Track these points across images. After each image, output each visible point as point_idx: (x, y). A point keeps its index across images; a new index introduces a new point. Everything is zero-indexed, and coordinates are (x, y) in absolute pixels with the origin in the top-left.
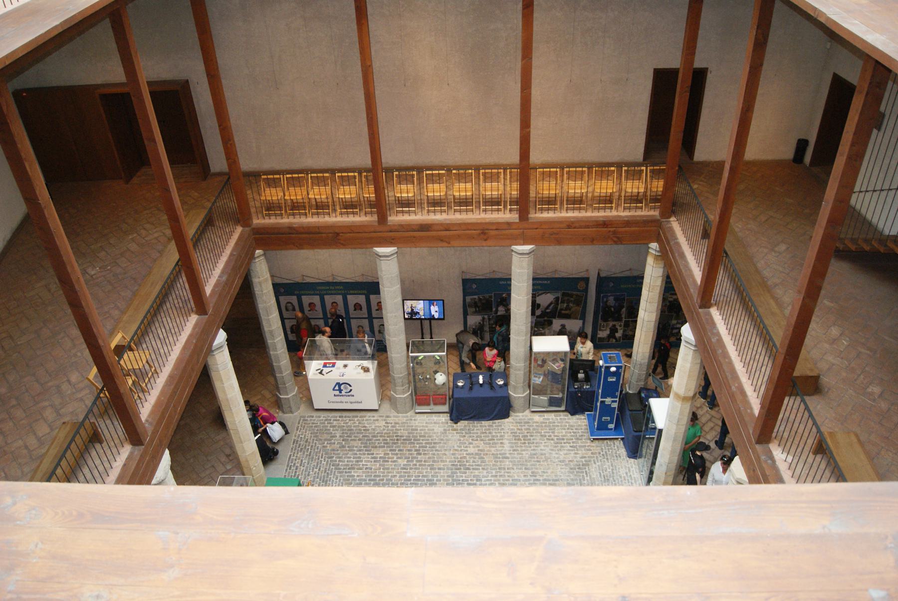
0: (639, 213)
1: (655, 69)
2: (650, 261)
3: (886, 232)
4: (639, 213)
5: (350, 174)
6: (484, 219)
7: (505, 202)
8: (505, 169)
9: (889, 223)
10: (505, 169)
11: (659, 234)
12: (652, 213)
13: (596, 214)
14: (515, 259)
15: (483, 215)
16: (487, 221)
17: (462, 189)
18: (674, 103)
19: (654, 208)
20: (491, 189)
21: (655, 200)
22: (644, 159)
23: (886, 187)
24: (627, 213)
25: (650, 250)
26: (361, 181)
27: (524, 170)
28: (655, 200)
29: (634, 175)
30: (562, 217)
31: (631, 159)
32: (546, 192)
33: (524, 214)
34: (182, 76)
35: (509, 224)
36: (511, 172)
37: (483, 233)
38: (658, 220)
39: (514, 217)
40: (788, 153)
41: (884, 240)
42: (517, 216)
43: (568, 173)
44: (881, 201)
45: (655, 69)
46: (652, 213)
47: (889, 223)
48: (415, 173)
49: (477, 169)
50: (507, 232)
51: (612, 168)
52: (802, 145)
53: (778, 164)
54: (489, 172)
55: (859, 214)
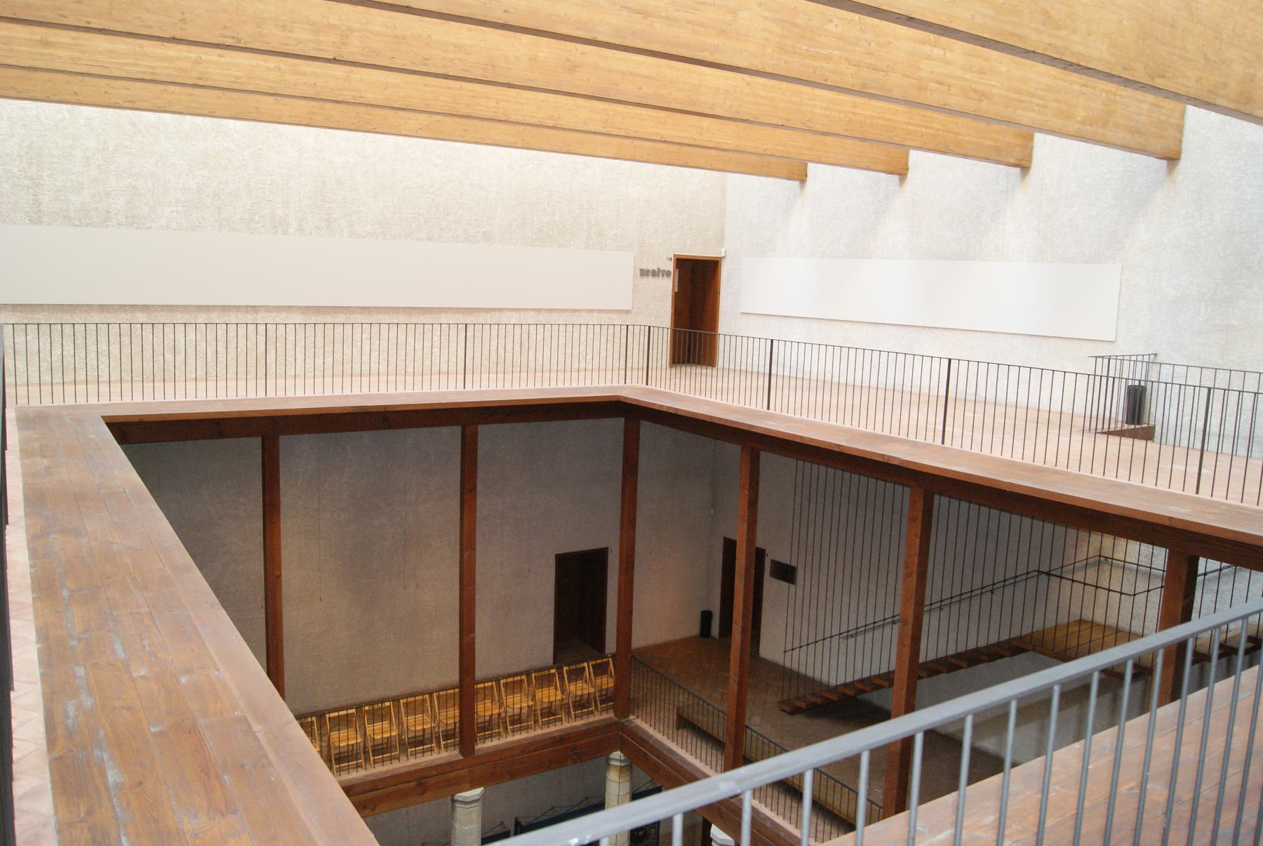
0: (592, 719)
1: (557, 556)
2: (613, 776)
3: (833, 683)
4: (592, 719)
5: (342, 713)
6: (381, 773)
7: (366, 752)
8: (431, 694)
9: (833, 674)
10: (431, 694)
11: (622, 738)
12: (605, 716)
13: (546, 730)
14: (460, 811)
15: (412, 761)
16: (423, 766)
17: (380, 731)
18: (582, 591)
19: (607, 710)
20: (417, 723)
21: (447, 736)
22: (555, 662)
23: (796, 644)
24: (579, 723)
25: (612, 763)
26: (561, 678)
27: (466, 689)
28: (447, 736)
29: (545, 680)
30: (508, 743)
31: (538, 663)
32: (378, 737)
33: (466, 746)
34: (552, 562)
35: (451, 765)
36: (438, 697)
37: (420, 784)
38: (616, 723)
39: (453, 754)
40: (694, 629)
41: (829, 689)
42: (457, 752)
43: (407, 704)
44: (868, 644)
45: (557, 556)
46: (605, 716)
47: (833, 674)
48: (314, 719)
49: (396, 700)
50: (451, 775)
51: (387, 704)
52: (706, 617)
53: (687, 641)
54: (412, 701)
55: (798, 674)
